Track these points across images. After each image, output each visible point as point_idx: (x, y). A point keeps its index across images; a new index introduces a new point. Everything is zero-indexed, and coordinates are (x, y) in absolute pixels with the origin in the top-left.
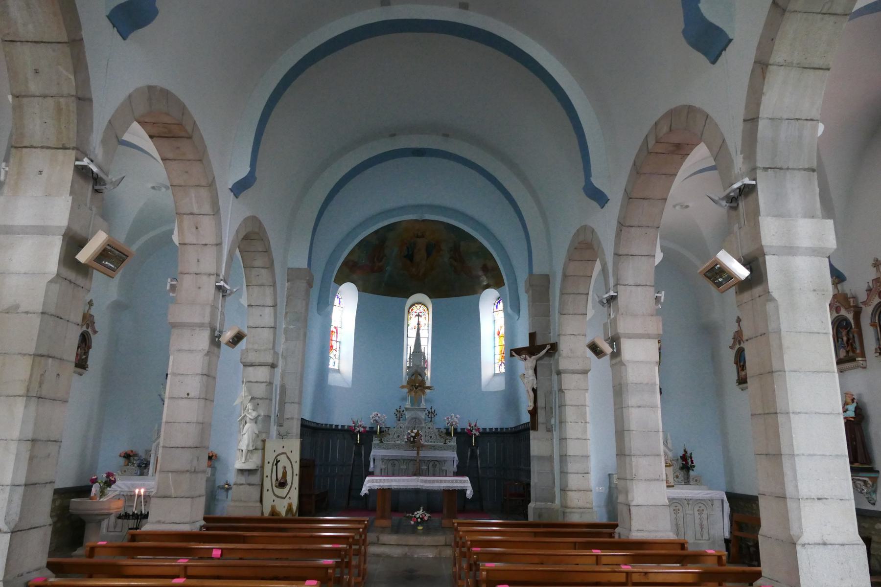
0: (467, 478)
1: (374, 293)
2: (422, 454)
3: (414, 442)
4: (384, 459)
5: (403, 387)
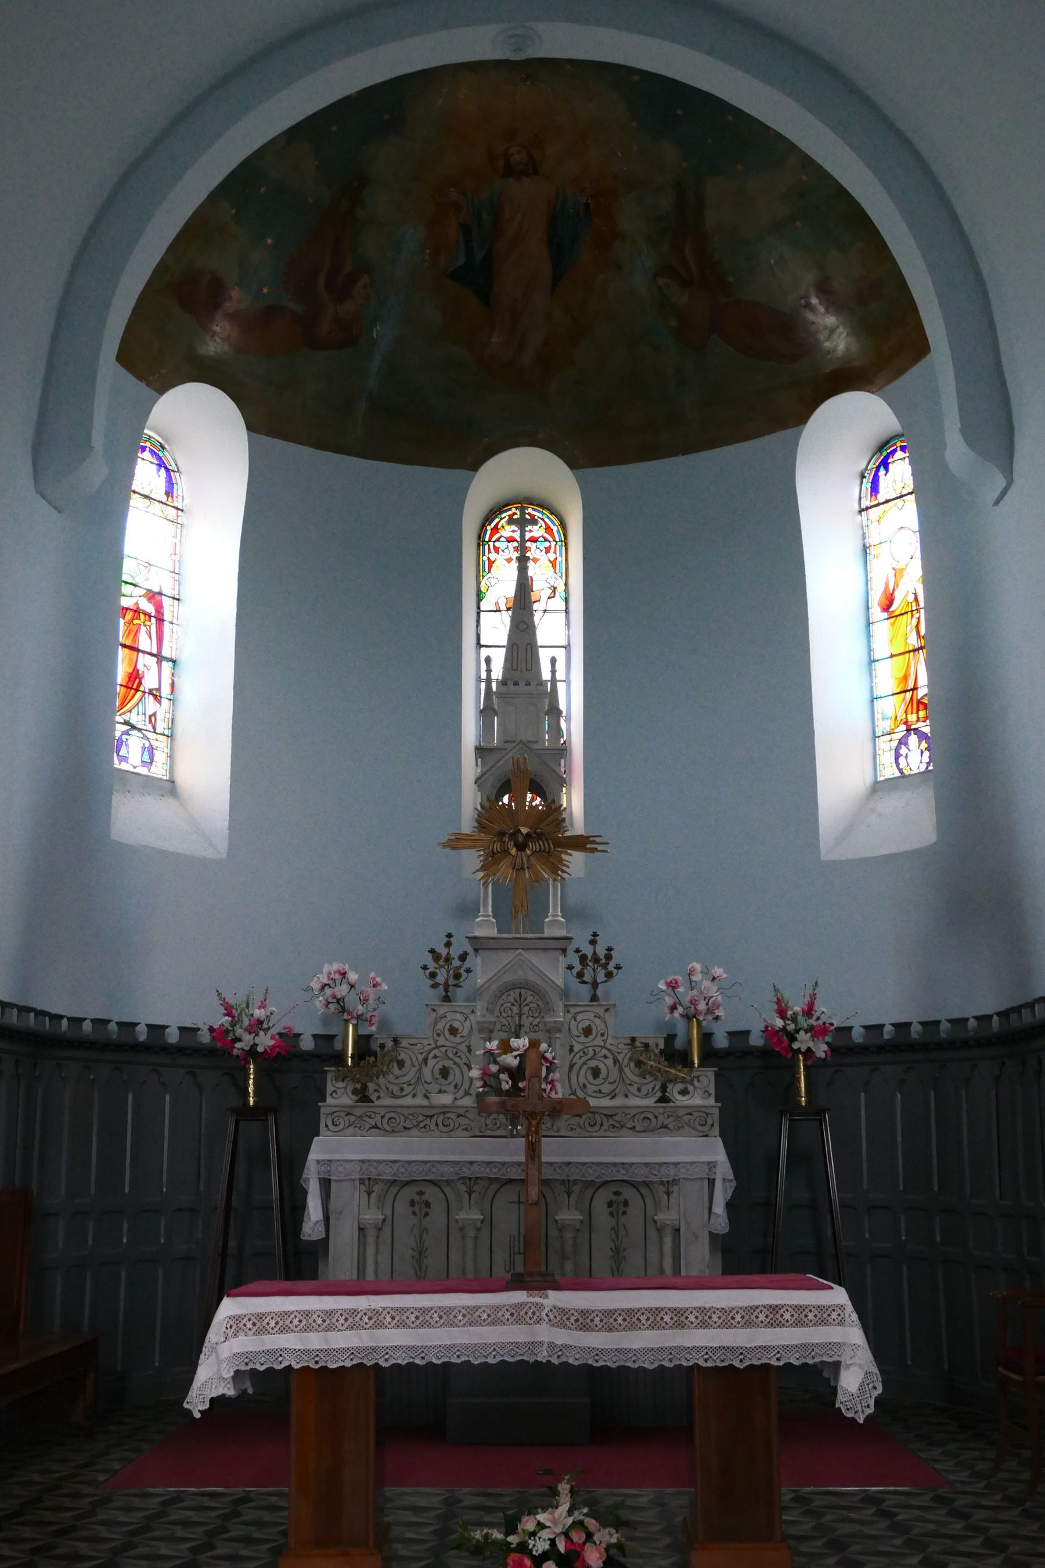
0: (838, 1296)
1: (321, 444)
2: (555, 1151)
3: (518, 1099)
4: (372, 1182)
5: (458, 842)
